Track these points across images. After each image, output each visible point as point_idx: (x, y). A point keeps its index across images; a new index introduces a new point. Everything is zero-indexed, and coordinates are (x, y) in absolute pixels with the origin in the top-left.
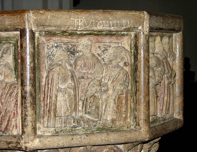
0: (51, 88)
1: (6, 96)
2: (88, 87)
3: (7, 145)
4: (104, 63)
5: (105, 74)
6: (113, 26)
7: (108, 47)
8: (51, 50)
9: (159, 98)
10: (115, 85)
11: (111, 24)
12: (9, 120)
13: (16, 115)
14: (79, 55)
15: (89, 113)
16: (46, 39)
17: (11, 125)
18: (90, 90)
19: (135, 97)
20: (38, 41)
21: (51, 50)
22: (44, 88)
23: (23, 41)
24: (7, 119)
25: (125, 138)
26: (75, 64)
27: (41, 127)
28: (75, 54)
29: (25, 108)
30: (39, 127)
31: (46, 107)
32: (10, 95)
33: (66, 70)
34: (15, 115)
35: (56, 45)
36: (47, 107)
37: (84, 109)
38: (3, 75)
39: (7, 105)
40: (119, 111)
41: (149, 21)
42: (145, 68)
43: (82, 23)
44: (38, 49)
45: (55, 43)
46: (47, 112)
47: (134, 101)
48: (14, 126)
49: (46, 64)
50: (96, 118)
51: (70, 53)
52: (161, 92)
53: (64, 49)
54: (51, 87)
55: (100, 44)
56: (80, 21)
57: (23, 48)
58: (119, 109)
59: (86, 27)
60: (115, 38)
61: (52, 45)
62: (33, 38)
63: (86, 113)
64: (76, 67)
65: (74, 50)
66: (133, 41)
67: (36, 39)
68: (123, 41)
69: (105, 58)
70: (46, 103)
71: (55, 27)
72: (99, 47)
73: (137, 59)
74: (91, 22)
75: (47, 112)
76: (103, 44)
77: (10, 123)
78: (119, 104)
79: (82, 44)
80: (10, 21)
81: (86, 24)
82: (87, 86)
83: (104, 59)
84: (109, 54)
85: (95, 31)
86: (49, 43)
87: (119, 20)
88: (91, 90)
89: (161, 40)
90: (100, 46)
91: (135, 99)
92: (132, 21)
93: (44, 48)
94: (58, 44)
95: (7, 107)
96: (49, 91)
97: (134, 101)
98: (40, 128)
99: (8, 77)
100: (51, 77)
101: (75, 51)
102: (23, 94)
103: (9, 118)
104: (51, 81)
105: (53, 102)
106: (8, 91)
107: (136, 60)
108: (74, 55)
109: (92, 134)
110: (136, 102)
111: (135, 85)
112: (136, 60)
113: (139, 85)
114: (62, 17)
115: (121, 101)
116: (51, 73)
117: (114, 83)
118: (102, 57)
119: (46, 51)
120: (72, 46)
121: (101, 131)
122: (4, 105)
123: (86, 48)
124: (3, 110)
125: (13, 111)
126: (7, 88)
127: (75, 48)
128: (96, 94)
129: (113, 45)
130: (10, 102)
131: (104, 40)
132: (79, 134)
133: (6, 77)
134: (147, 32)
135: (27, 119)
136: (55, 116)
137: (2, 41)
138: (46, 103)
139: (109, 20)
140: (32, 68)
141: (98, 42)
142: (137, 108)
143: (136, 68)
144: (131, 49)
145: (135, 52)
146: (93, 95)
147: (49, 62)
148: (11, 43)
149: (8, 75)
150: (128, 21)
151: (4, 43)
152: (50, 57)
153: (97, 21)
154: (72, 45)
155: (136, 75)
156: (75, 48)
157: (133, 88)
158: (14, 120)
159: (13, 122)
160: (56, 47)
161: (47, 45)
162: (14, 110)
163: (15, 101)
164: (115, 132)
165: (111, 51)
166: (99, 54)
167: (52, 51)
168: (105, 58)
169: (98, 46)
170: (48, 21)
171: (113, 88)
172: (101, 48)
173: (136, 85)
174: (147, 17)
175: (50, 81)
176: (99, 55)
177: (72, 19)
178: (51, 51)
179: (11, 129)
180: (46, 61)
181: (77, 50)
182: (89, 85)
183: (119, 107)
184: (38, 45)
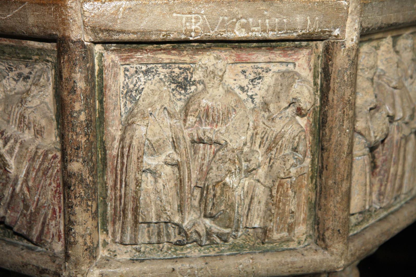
0: (127, 165)
1: (36, 175)
2: (213, 161)
3: (38, 273)
4: (252, 106)
5: (252, 131)
6: (273, 30)
7: (263, 71)
8: (135, 79)
9: (378, 170)
10: (273, 156)
11: (268, 25)
12: (44, 223)
13: (58, 214)
14: (196, 90)
15: (211, 217)
16: (120, 57)
17: (48, 232)
18: (214, 168)
19: (318, 179)
20: (100, 61)
21: (135, 79)
22: (115, 162)
23: (62, 65)
24: (40, 219)
25: (291, 268)
26: (185, 112)
27: (109, 242)
28: (188, 87)
29: (69, 207)
30: (104, 240)
31: (118, 202)
32: (44, 174)
33: (162, 125)
34: (56, 214)
35: (144, 68)
36: (120, 204)
37: (203, 206)
38: (32, 130)
39: (40, 192)
40: (280, 211)
41: (361, 14)
42: (343, 121)
43: (199, 24)
44: (102, 79)
45: (141, 64)
46: (120, 213)
47: (316, 187)
48: (55, 235)
49: (123, 109)
50: (227, 227)
51: (177, 86)
52: (384, 157)
53: (163, 77)
54: (127, 162)
55: (245, 65)
56: (193, 21)
57: (64, 80)
58: (279, 208)
59: (209, 32)
60: (279, 52)
61: (135, 69)
62: (84, 58)
63: (205, 216)
64: (188, 118)
65: (185, 79)
66: (320, 59)
67: (96, 56)
68: (299, 59)
69: (256, 94)
70: (118, 194)
71: (134, 33)
72: (244, 72)
73: (328, 100)
74: (220, 21)
75: (122, 213)
76: (252, 65)
77: (46, 229)
78: (280, 198)
79: (203, 66)
80: (38, 16)
81: (209, 26)
82: (211, 158)
83: (254, 97)
84: (266, 87)
85: (101, 102)
86: (128, 64)
87: (288, 15)
88: (218, 168)
89: (394, 45)
90: (244, 69)
91: (318, 184)
92: (317, 18)
93: (116, 75)
94: (150, 66)
95: (39, 195)
96: (124, 170)
97: (316, 187)
98: (108, 244)
99: (41, 135)
100: (127, 141)
101: (187, 81)
102: (66, 178)
103: (45, 218)
104: (127, 149)
105: (131, 194)
106: (41, 165)
107: (324, 102)
108: (185, 89)
109: (219, 259)
110: (321, 191)
111: (320, 156)
112: (324, 102)
113: (328, 157)
114: (152, 11)
115: (284, 191)
116: (129, 132)
117: (272, 152)
118: (250, 94)
119: (121, 82)
120: (181, 71)
121: (238, 250)
122: (33, 192)
123: (212, 76)
124: (32, 202)
125: (52, 207)
126: (39, 158)
127: (189, 74)
128: (227, 180)
129: (275, 68)
130: (44, 188)
131: (254, 57)
132: (191, 257)
133: (38, 133)
134: (352, 40)
135: (73, 231)
136: (136, 222)
137: (31, 54)
138: (118, 194)
139: (264, 16)
140: (84, 124)
141: (242, 62)
142: (322, 204)
143: (323, 119)
144: (315, 77)
145: (324, 85)
146: (221, 181)
147: (129, 106)
148: (48, 61)
149: (41, 131)
150: (308, 18)
151: (36, 60)
152: (131, 95)
153: (235, 20)
154: (180, 68)
155: (323, 133)
156: (189, 74)
157: (316, 160)
158: (54, 222)
159: (51, 227)
160: (146, 73)
161: (125, 68)
162: (53, 204)
163: (55, 185)
164: (270, 253)
165: (269, 79)
166: (243, 86)
167: (137, 82)
168: (256, 94)
169: (240, 70)
170: (119, 21)
171: (269, 163)
172: (247, 74)
173: (322, 156)
174: (356, 7)
175: (126, 150)
176: (242, 88)
177: (175, 15)
178: (135, 82)
179: (50, 241)
180: (122, 104)
181: (192, 80)
182: (214, 157)
183: (279, 202)
184: (101, 71)
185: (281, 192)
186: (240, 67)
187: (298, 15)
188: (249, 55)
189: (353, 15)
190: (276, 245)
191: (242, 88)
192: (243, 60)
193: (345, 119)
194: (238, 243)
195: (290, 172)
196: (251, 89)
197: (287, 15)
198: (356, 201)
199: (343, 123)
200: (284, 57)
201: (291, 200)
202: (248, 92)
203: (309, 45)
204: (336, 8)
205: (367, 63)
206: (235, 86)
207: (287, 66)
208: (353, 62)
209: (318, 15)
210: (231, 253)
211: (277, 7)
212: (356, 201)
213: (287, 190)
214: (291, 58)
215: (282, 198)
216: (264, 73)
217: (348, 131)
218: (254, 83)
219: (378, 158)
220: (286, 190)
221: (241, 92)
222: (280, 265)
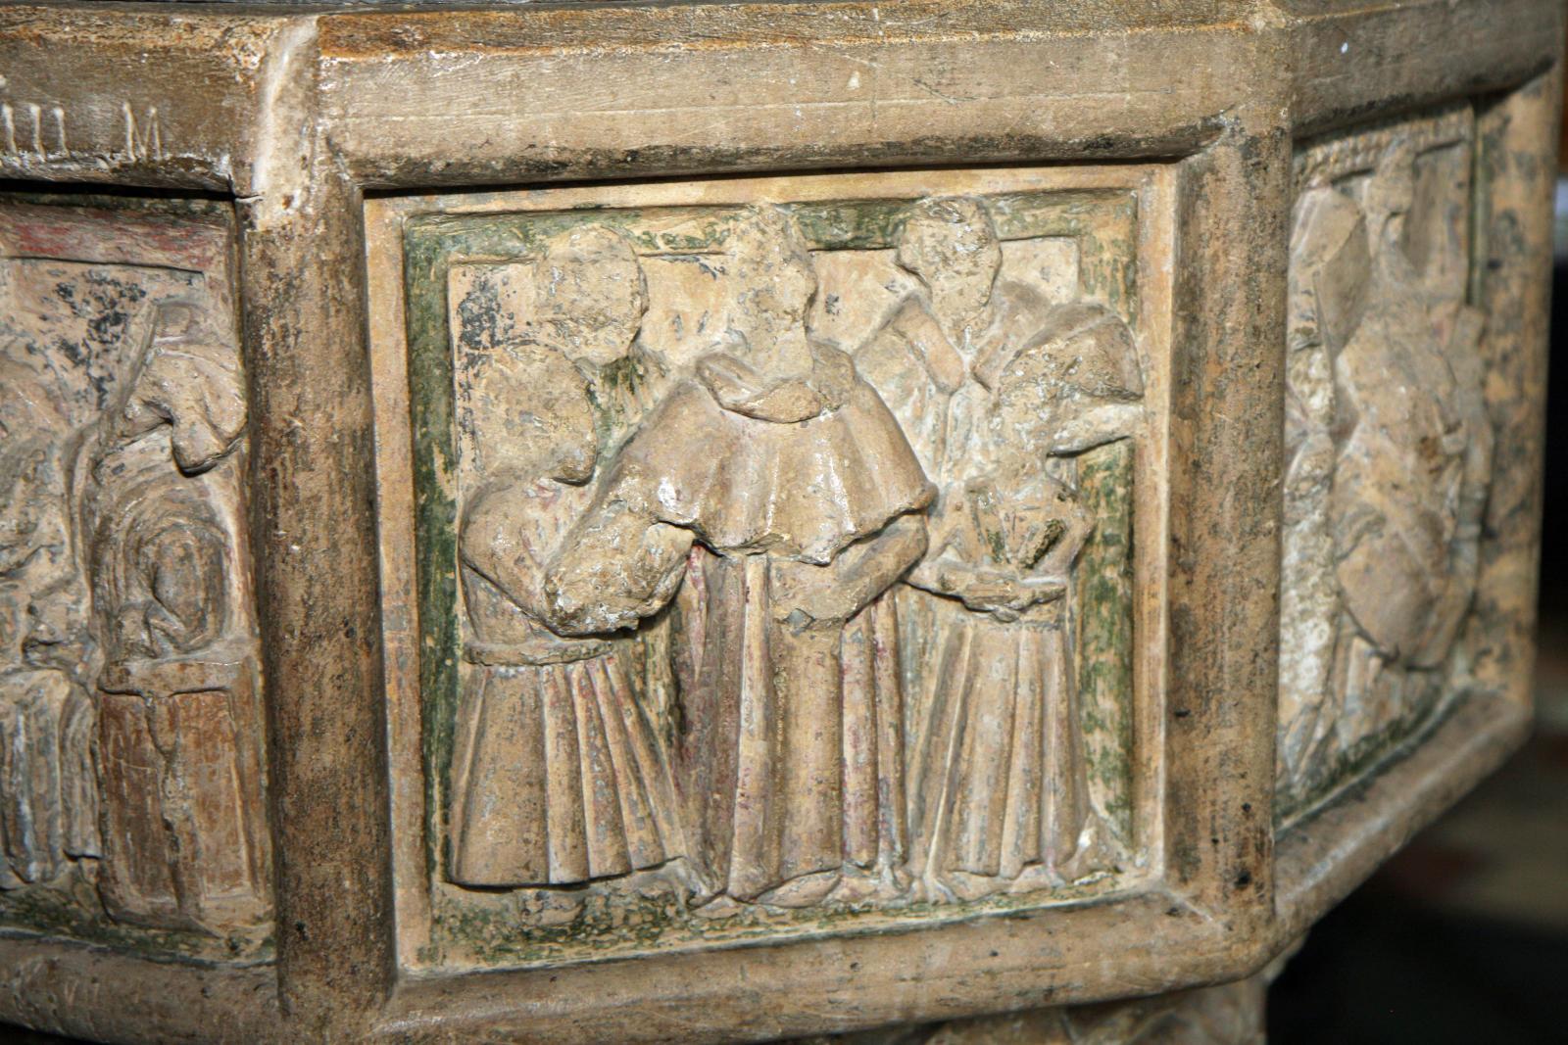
7: (121, 295)
25: (161, 1029)
72: (65, 292)
76: (86, 268)
78: (118, 765)
87: (67, 98)
90: (64, 280)
92: (153, 111)
115: (127, 739)
118: (96, 373)
134: (288, 201)
150: (126, 108)
166: (72, 342)
169: (52, 282)
172: (77, 298)
185: (116, 741)
186: (50, 273)
187: (96, 97)
188: (56, 231)
189: (291, 108)
190: (155, 936)
191: (70, 350)
192: (43, 250)
193: (281, 502)
194: (44, 899)
195: (128, 673)
196: (97, 356)
197: (63, 95)
198: (490, 837)
199: (275, 514)
200: (164, 249)
201: (161, 776)
202: (89, 365)
203: (213, 209)
204: (211, 77)
205: (573, 302)
206: (47, 340)
207: (190, 283)
208: (289, 285)
209: (155, 100)
210: (21, 930)
211: (32, 62)
212: (490, 837)
213: (139, 741)
214: (185, 254)
215: (123, 763)
216: (124, 300)
217: (295, 548)
218: (107, 337)
219: (689, 692)
220: (133, 737)
221: (68, 363)
222: (125, 1010)
